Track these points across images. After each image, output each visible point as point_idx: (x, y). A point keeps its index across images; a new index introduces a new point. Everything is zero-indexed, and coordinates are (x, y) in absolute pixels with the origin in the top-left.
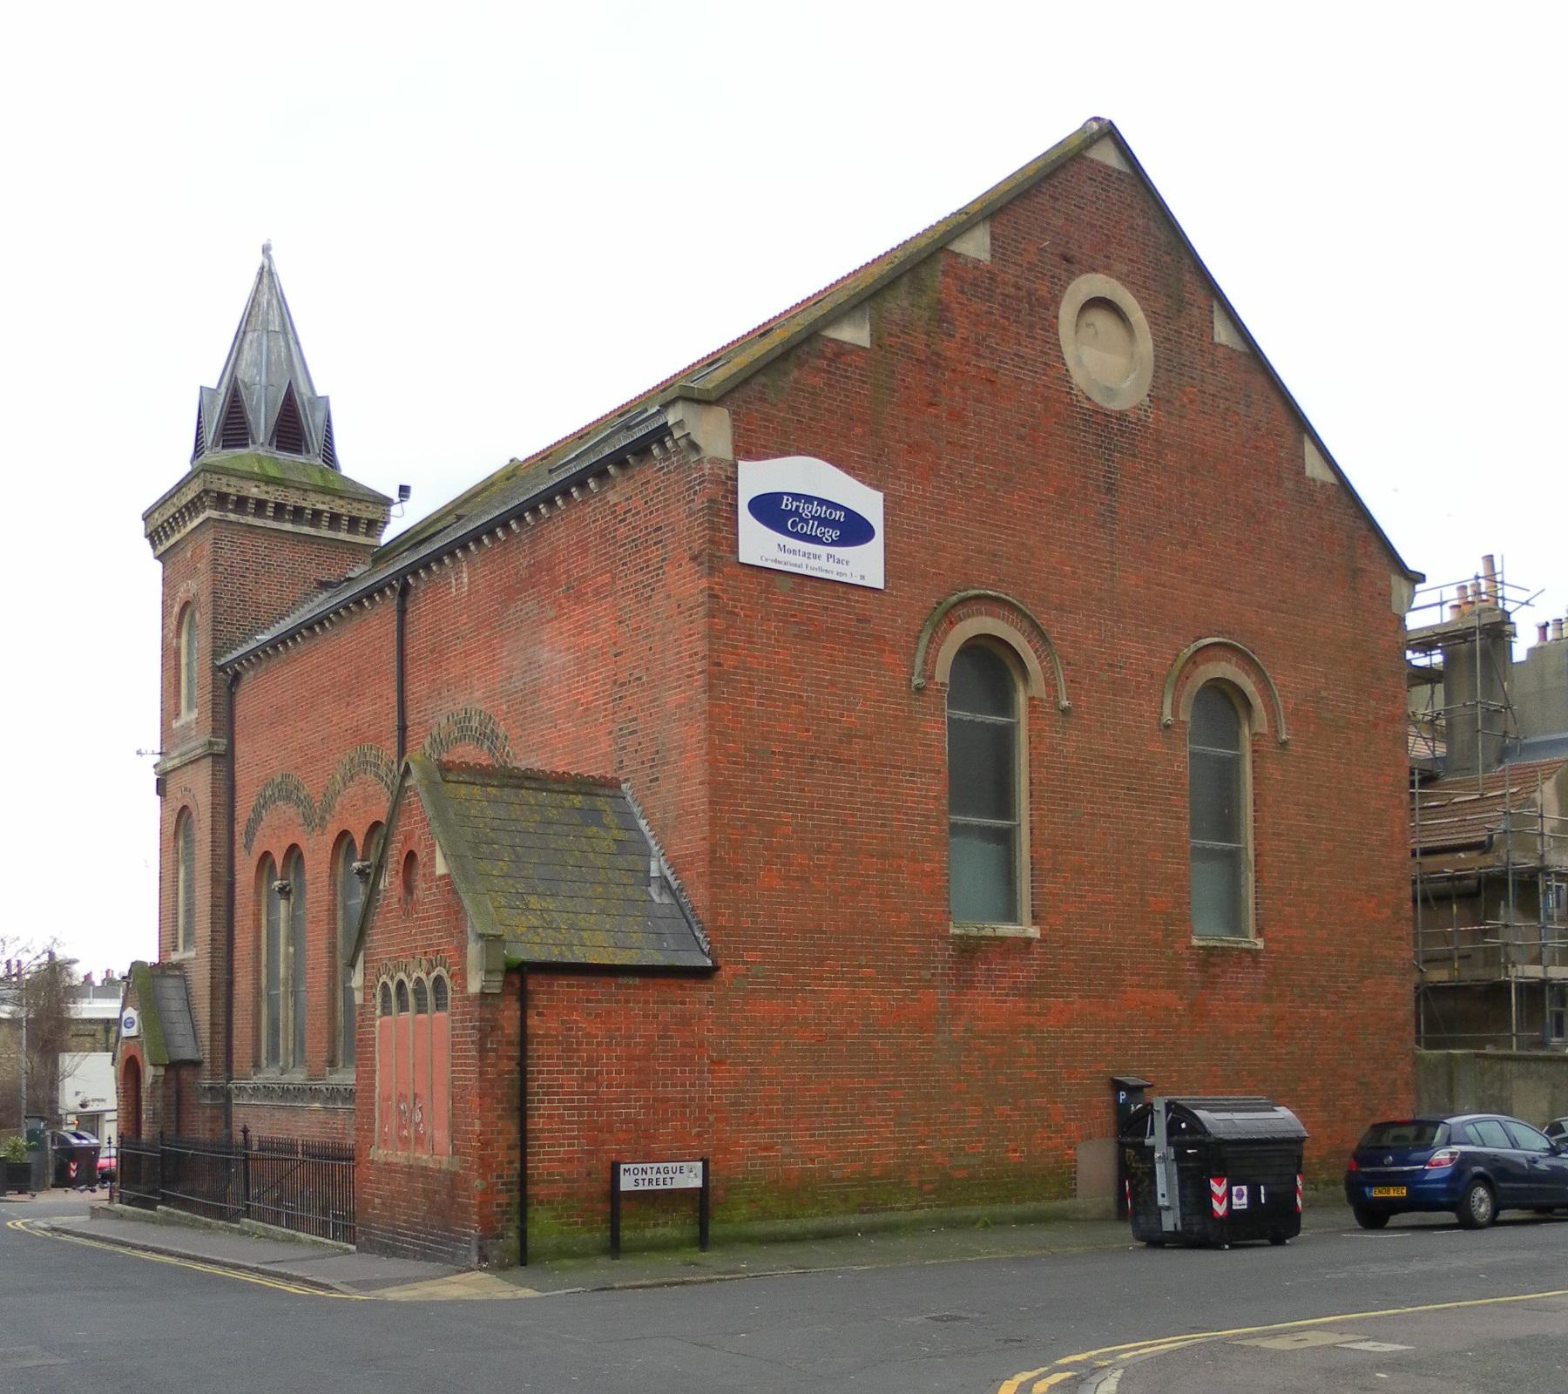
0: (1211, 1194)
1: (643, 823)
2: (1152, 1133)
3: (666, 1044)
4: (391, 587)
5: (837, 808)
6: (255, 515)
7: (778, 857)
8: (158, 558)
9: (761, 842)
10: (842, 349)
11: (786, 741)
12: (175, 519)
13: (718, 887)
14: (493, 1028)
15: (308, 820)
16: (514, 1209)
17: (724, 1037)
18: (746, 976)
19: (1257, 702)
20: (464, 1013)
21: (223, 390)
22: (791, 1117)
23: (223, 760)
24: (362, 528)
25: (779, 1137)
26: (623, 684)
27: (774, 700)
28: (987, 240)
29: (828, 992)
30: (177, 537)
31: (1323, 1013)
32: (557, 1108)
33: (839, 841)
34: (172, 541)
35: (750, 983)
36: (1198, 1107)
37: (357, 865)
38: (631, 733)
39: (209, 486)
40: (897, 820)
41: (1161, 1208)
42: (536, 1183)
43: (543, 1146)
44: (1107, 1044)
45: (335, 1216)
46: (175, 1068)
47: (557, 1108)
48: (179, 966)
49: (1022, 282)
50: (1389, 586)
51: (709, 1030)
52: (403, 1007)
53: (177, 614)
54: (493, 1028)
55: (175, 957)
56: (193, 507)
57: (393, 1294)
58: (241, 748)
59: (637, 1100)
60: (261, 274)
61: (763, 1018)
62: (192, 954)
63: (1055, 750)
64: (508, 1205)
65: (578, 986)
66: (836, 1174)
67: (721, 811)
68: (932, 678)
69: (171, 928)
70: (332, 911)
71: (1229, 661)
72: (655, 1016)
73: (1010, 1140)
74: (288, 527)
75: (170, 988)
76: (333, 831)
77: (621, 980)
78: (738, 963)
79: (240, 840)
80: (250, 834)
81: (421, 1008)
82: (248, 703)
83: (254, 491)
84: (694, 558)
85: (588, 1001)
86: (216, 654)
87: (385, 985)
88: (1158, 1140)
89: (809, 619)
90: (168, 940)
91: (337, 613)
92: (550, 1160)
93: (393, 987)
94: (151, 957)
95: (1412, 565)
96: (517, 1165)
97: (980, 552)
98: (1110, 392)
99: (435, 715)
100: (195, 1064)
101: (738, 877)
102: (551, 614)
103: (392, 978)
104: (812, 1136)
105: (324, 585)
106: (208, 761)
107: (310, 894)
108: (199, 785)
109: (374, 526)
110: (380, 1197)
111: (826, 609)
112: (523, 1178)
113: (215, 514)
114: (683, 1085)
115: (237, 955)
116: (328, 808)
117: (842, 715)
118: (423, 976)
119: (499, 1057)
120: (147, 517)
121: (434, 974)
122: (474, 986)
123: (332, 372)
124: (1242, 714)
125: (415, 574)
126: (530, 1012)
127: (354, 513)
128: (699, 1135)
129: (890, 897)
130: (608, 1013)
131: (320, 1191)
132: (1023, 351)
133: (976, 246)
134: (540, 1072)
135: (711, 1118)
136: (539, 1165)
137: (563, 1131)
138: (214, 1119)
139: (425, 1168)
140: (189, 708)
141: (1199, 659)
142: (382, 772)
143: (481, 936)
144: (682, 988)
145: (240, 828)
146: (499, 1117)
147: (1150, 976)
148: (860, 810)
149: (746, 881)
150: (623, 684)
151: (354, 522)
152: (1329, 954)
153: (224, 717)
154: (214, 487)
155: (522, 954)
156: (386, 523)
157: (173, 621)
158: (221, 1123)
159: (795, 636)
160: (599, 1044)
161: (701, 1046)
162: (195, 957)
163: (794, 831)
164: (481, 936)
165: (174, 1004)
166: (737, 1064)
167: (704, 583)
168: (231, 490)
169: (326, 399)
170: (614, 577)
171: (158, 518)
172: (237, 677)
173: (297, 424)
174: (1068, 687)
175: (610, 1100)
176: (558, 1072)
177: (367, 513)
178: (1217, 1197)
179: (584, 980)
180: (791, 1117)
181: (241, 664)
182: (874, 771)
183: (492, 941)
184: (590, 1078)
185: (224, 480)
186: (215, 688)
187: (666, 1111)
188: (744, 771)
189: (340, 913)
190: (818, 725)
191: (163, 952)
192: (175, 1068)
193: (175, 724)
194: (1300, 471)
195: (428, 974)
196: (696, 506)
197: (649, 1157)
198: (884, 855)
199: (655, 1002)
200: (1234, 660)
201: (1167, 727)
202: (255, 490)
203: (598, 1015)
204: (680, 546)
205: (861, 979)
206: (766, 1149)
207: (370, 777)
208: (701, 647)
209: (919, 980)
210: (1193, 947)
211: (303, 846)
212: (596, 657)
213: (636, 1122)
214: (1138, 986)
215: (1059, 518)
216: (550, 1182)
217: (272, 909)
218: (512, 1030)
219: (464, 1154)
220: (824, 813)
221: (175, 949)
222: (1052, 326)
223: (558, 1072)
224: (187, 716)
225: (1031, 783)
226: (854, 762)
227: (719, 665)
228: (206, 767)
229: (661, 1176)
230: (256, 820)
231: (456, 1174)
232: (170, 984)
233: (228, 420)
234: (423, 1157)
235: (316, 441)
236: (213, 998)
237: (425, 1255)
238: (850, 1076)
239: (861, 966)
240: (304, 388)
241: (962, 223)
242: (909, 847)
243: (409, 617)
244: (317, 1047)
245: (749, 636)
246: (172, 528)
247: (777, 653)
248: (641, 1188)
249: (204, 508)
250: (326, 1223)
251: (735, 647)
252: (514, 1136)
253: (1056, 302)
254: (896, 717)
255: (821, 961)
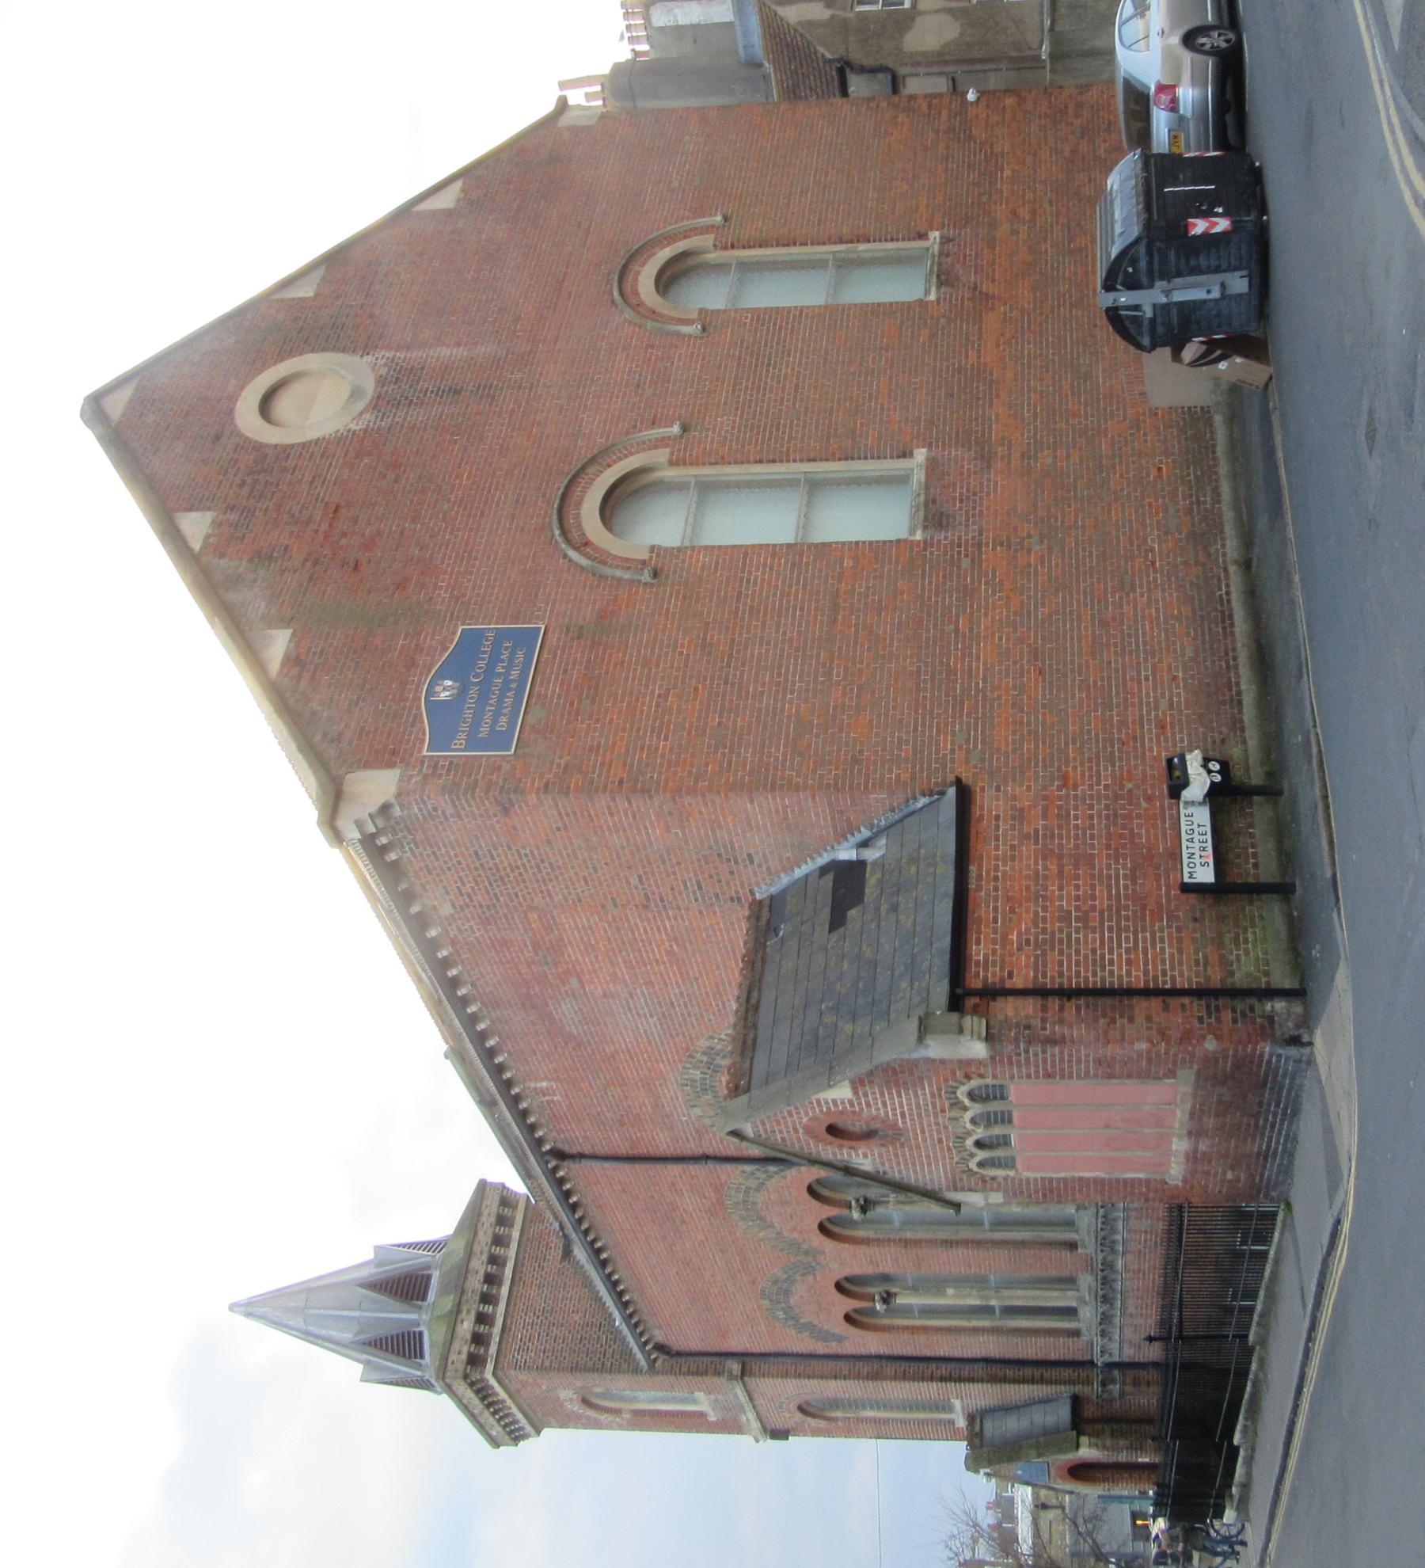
0: (1205, 235)
1: (798, 873)
2: (1137, 308)
3: (1044, 836)
4: (555, 1169)
5: (781, 656)
6: (492, 1325)
7: (834, 716)
8: (538, 1432)
9: (817, 735)
10: (293, 660)
11: (708, 710)
12: (501, 1418)
13: (866, 783)
14: (1028, 1027)
15: (809, 1270)
16: (1240, 1005)
17: (1036, 773)
18: (968, 751)
19: (681, 246)
20: (1011, 1063)
21: (365, 1357)
22: (1126, 700)
23: (748, 1363)
24: (507, 1212)
25: (1149, 713)
26: (646, 896)
27: (662, 723)
28: (193, 515)
29: (985, 664)
30: (514, 1410)
31: (1007, 173)
32: (1120, 956)
33: (818, 655)
34: (519, 1416)
35: (975, 746)
36: (1109, 254)
37: (856, 1215)
38: (700, 888)
39: (461, 1373)
40: (796, 596)
41: (1223, 296)
42: (1208, 979)
43: (1164, 973)
44: (1042, 380)
45: (1234, 1298)
46: (1081, 1422)
47: (1120, 956)
48: (971, 1419)
49: (238, 480)
50: (568, 128)
51: (1029, 788)
52: (1004, 1141)
53: (594, 1412)
54: (1028, 1027)
55: (961, 1423)
56: (483, 1392)
57: (1349, 1140)
58: (736, 1344)
59: (1109, 867)
60: (249, 1315)
61: (1014, 732)
62: (957, 1404)
63: (725, 438)
64: (1234, 1011)
65: (979, 932)
66: (1189, 653)
67: (782, 779)
68: (644, 563)
69: (924, 1426)
70: (906, 1243)
71: (638, 273)
72: (1013, 848)
73: (1148, 475)
74: (505, 1290)
75: (992, 1428)
76: (818, 1240)
77: (972, 885)
78: (953, 761)
79: (833, 1348)
80: (826, 1336)
81: (1006, 1119)
82: (689, 1336)
83: (467, 1326)
84: (506, 811)
85: (995, 921)
86: (637, 1370)
87: (981, 1164)
88: (1147, 300)
89: (576, 688)
90: (946, 1431)
91: (586, 1232)
92: (1181, 964)
93: (981, 1155)
94: (961, 1448)
95: (548, 107)
96: (1186, 1000)
97: (513, 516)
98: (356, 393)
99: (689, 1113)
100: (1076, 1402)
101: (856, 761)
102: (574, 982)
103: (972, 1155)
104: (1147, 678)
105: (567, 1253)
106: (752, 1382)
107: (886, 1267)
108: (781, 1392)
109: (507, 1200)
110: (1224, 1173)
111: (565, 671)
112: (1199, 993)
113: (490, 1367)
114: (1091, 817)
115: (957, 1353)
116: (795, 1246)
117: (681, 653)
118: (968, 1115)
119: (1061, 1022)
120: (495, 1443)
121: (967, 1102)
122: (978, 1049)
123: (349, 1246)
124: (691, 262)
125: (540, 1142)
126: (1008, 985)
127: (493, 1219)
128: (1149, 799)
129: (880, 601)
130: (1009, 899)
131: (1220, 1251)
132: (307, 478)
133: (196, 526)
134: (1078, 973)
135: (1129, 786)
136: (1185, 976)
137: (1145, 949)
138: (1136, 1383)
139: (1192, 1115)
140: (695, 1401)
141: (634, 302)
142: (752, 1183)
143: (921, 1039)
144: (980, 819)
145: (821, 1348)
146: (1131, 1020)
147: (967, 339)
148: (784, 633)
149: (861, 752)
150: (646, 896)
151: (501, 1221)
152: (946, 170)
153: (707, 1362)
154: (460, 1367)
155: (941, 992)
156: (504, 1186)
157: (603, 1418)
158: (1142, 1373)
159: (593, 701)
160: (1045, 909)
161: (1045, 798)
162: (962, 1400)
163: (807, 700)
164: (921, 1039)
165: (1013, 1425)
166: (1067, 761)
167: (533, 799)
168: (465, 1349)
169: (377, 1248)
170: (531, 908)
171: (496, 1431)
172: (661, 1348)
173: (404, 1284)
174: (660, 427)
175: (1110, 897)
176: (1078, 952)
177: (492, 1206)
178: (1208, 228)
179: (972, 927)
180: (1126, 700)
181: (646, 1343)
182: (743, 619)
183: (925, 1029)
184: (1084, 919)
185: (453, 1357)
186: (671, 1371)
187: (1121, 836)
188: (739, 754)
189: (909, 1235)
190: (691, 678)
191: (955, 1435)
192: (1081, 1422)
193: (712, 1418)
194: (449, 213)
195: (965, 1109)
196: (450, 810)
197: (1175, 855)
198: (835, 607)
199: (997, 848)
200: (637, 268)
201: (704, 329)
202: (466, 1325)
203: (1012, 910)
204: (493, 827)
205: (971, 630)
206: (1163, 727)
207: (760, 1198)
208: (602, 801)
209: (973, 569)
210: (938, 300)
211: (839, 1275)
212: (618, 930)
213: (1133, 870)
214: (979, 351)
215: (482, 438)
216: (1206, 964)
217: (906, 1311)
218: (1028, 1007)
219: (1175, 1063)
220: (787, 670)
221: (951, 1422)
222: (284, 451)
223: (1078, 952)
224: (702, 1402)
225: (760, 461)
226: (733, 640)
227: (621, 781)
228: (756, 1383)
229: (1196, 836)
230: (810, 1327)
231: (1198, 1074)
232: (990, 1428)
233: (395, 1351)
234: (1180, 1116)
235: (425, 1256)
236: (1005, 1380)
237: (1293, 1111)
238: (1079, 641)
239: (957, 631)
240: (363, 1273)
241: (172, 537)
242: (826, 583)
243: (587, 1150)
244: (1060, 1263)
245: (591, 749)
246: (506, 1416)
247: (611, 720)
248: (1211, 861)
249: (483, 1380)
250: (1253, 1254)
251: (603, 764)
252: (1155, 1003)
253: (259, 447)
254: (684, 598)
255: (951, 672)
